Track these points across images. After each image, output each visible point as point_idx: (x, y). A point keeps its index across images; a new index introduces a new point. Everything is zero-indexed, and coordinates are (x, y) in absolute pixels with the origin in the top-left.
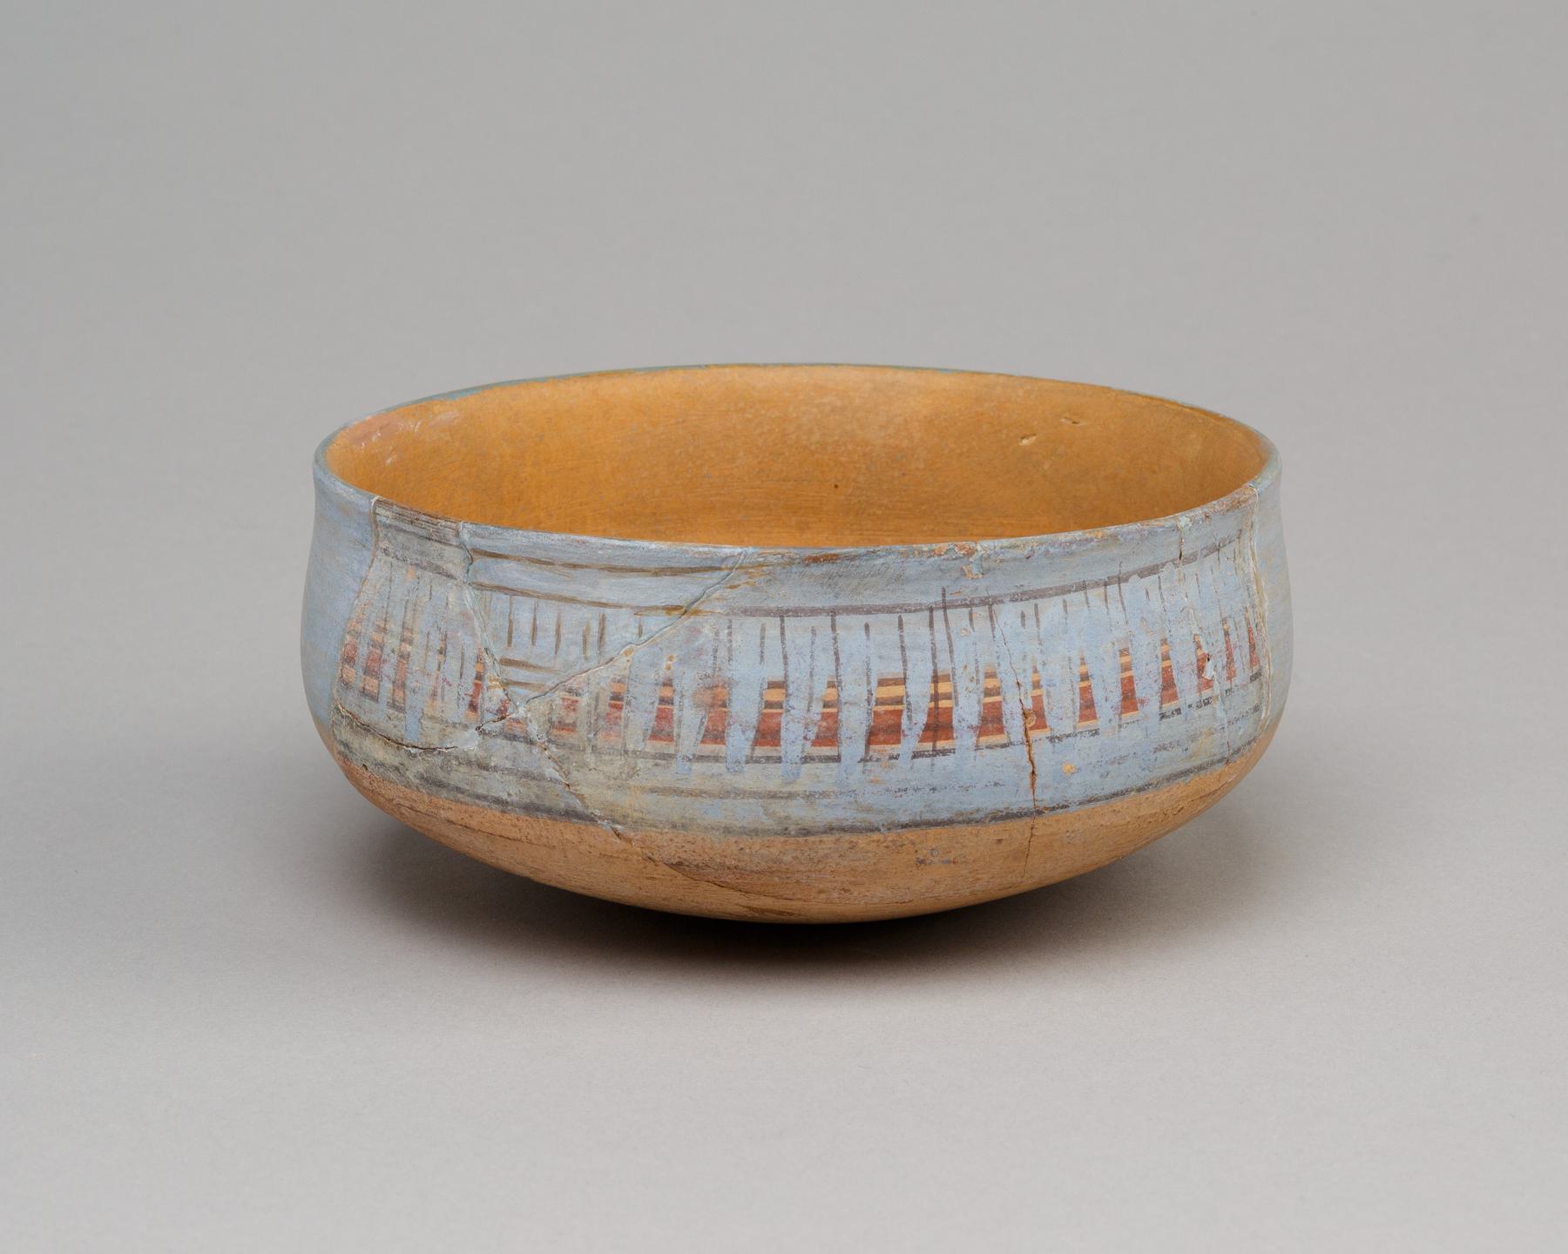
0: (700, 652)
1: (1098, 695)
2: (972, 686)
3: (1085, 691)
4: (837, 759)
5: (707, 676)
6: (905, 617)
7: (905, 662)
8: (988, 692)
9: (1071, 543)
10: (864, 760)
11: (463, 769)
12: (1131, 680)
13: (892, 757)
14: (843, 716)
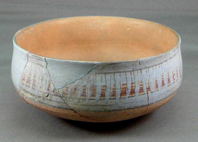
0: (90, 81)
1: (158, 84)
2: (138, 84)
3: (156, 84)
4: (115, 99)
5: (92, 85)
6: (127, 73)
7: (127, 81)
8: (141, 85)
9: (154, 58)
10: (120, 99)
11: (46, 100)
12: (163, 80)
13: (125, 98)
14: (116, 91)
